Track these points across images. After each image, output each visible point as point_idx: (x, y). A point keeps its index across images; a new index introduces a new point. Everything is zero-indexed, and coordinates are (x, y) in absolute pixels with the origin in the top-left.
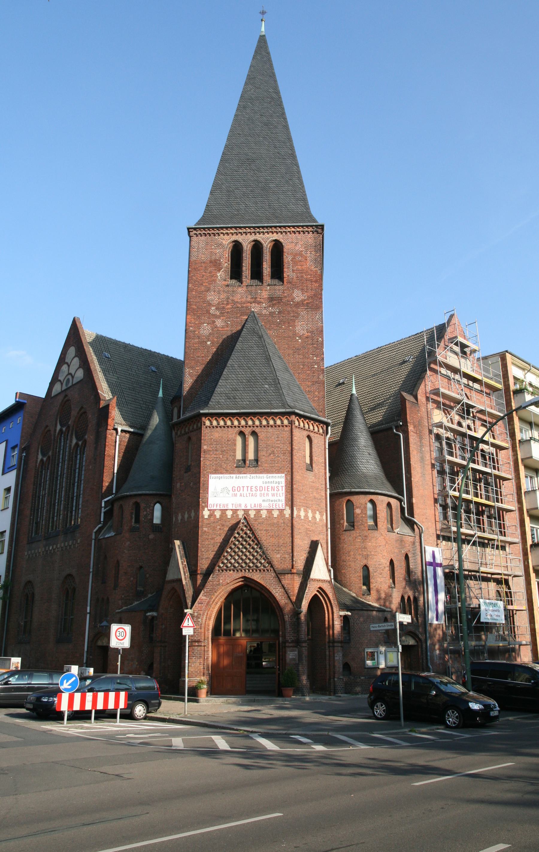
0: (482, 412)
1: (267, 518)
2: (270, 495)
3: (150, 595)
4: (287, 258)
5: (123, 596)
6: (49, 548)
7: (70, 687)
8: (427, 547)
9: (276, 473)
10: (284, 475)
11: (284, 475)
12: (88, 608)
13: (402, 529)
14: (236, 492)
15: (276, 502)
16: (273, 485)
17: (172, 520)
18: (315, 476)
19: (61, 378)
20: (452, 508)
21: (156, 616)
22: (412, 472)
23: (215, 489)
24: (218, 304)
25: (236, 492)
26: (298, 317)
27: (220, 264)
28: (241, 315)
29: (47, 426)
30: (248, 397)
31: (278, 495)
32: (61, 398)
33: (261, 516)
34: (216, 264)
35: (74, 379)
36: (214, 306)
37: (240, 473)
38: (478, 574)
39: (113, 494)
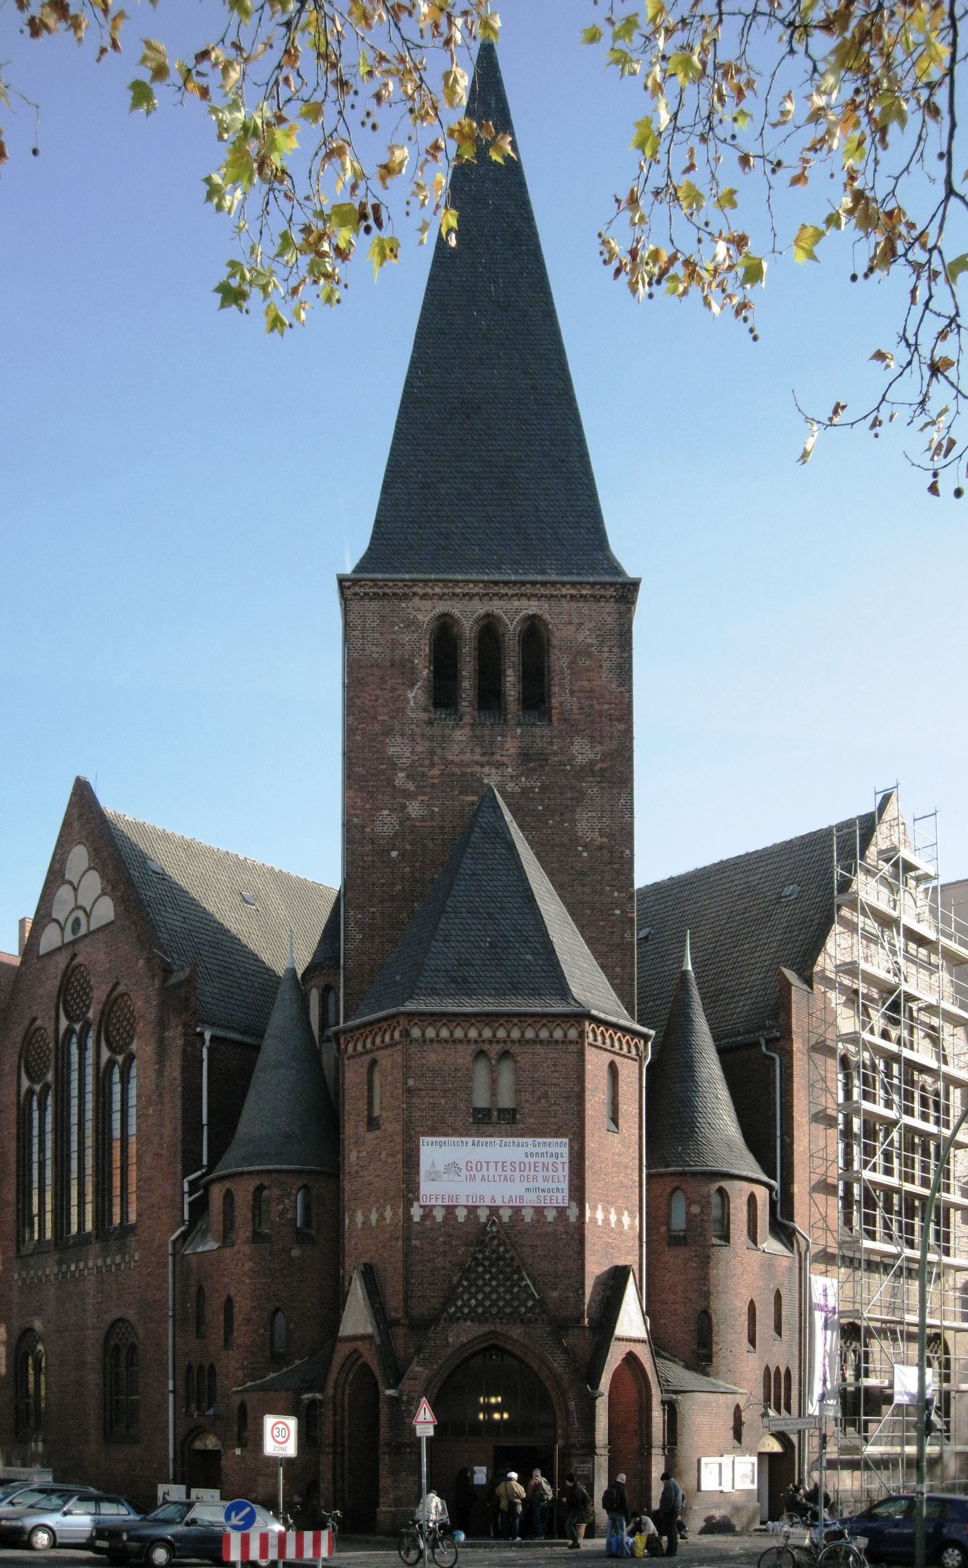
0: (931, 1009)
1: (532, 1225)
2: (540, 1179)
3: (297, 1362)
4: (559, 661)
5: (245, 1363)
6: (69, 1267)
7: (242, 1523)
8: (812, 1276)
9: (552, 1137)
10: (566, 1140)
11: (566, 1140)
12: (171, 1383)
13: (771, 1245)
14: (474, 1172)
15: (551, 1194)
16: (545, 1160)
17: (344, 1223)
18: (622, 1141)
19: (59, 912)
20: (864, 1204)
21: (320, 1401)
22: (795, 1133)
23: (433, 1165)
24: (412, 765)
25: (474, 1172)
26: (582, 801)
27: (413, 669)
28: (461, 793)
29: (34, 1019)
30: (492, 980)
31: (556, 1180)
32: (62, 960)
33: (523, 1220)
34: (404, 668)
35: (92, 920)
36: (402, 770)
37: (482, 1135)
38: (898, 1328)
39: (202, 1167)
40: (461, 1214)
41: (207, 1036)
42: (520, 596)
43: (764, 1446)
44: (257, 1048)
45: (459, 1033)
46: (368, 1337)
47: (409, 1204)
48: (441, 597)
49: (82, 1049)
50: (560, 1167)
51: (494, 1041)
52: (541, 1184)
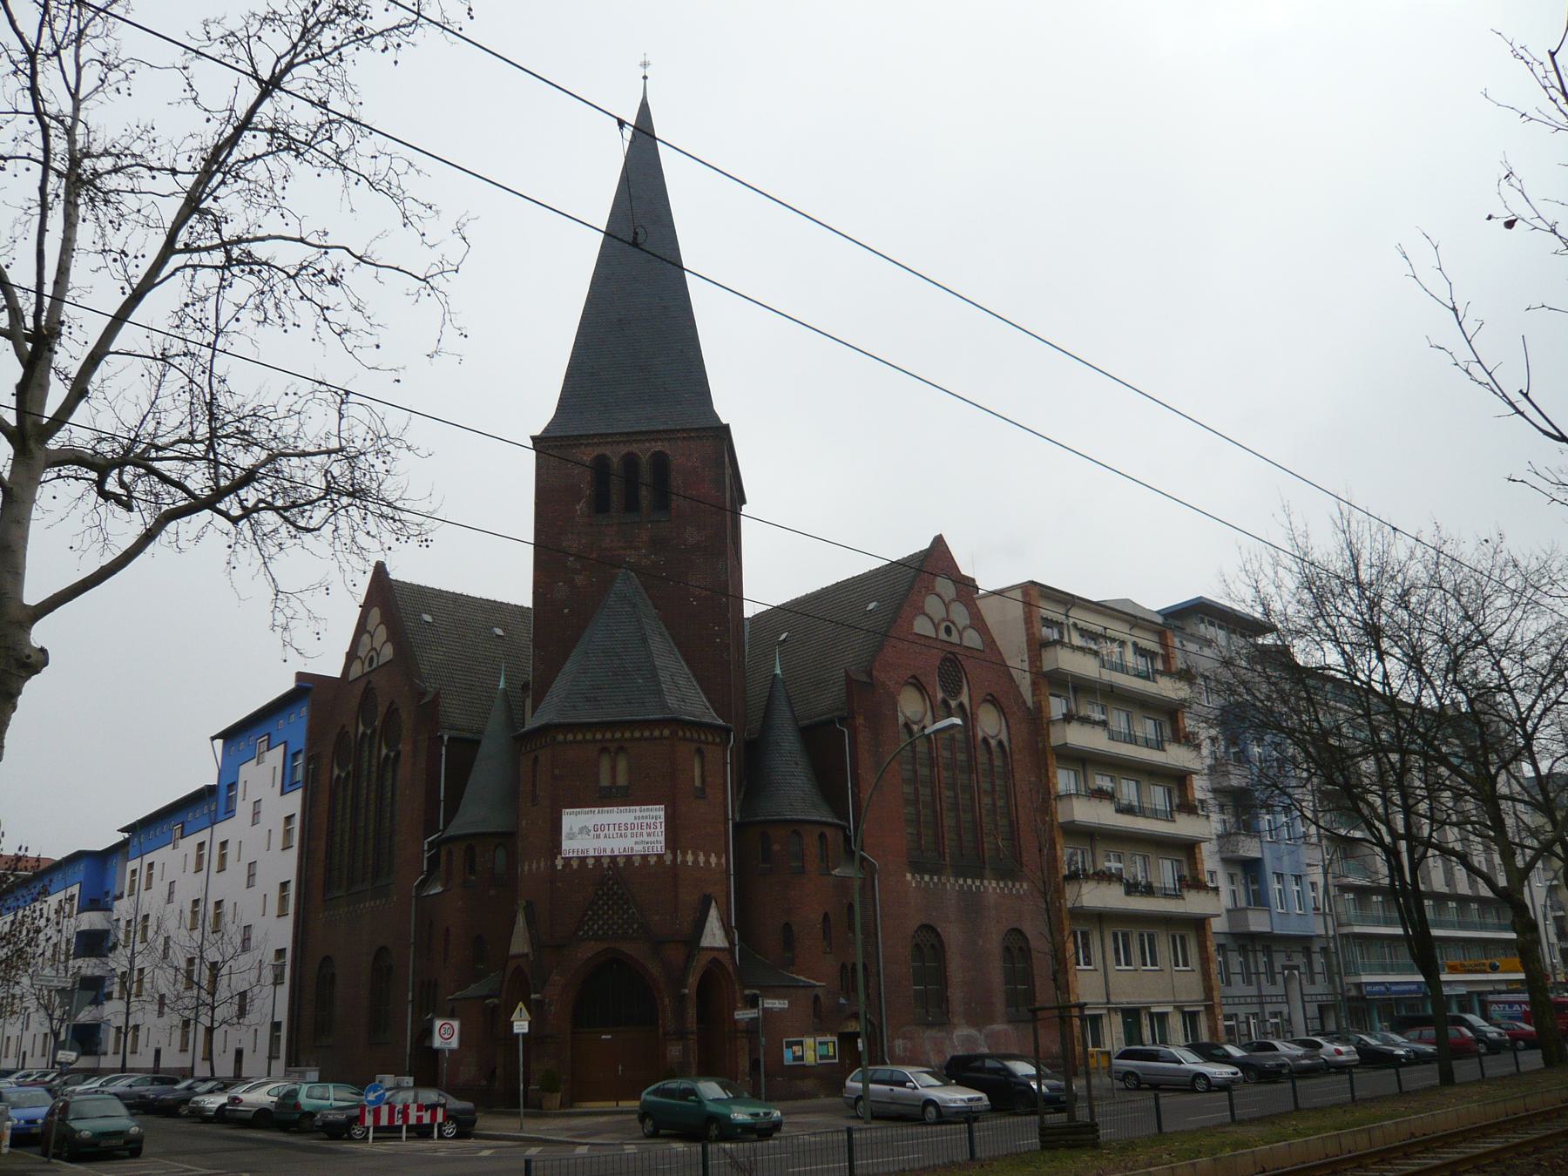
19: (362, 653)
40: (591, 862)
44: (479, 742)
45: (589, 736)
46: (526, 955)
48: (598, 445)
49: (371, 746)
51: (612, 740)
52: (646, 838)
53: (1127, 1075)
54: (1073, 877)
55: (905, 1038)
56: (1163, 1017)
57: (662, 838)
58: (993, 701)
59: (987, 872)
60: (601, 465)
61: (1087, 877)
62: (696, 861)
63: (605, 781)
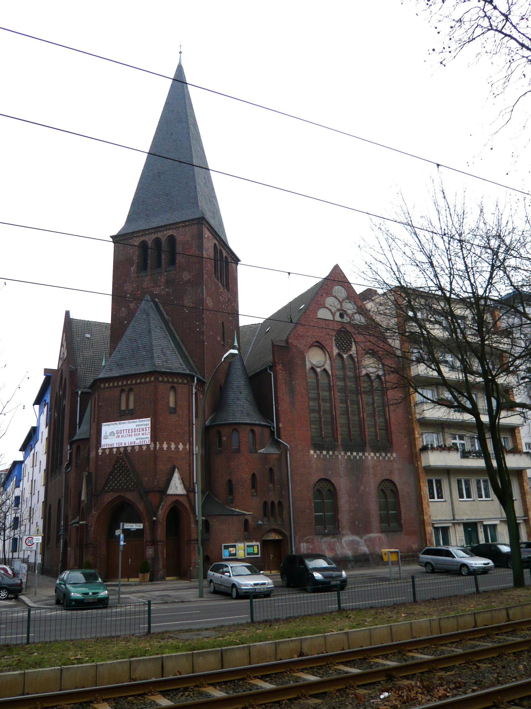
2: (141, 434)
4: (179, 248)
11: (150, 419)
12: (62, 522)
16: (143, 427)
23: (106, 433)
36: (129, 294)
40: (115, 450)
41: (80, 392)
42: (166, 230)
43: (269, 537)
47: (97, 449)
48: (142, 236)
50: (147, 429)
51: (127, 385)
52: (141, 436)
53: (427, 564)
54: (425, 449)
55: (307, 542)
56: (495, 526)
57: (149, 436)
58: (373, 353)
59: (368, 447)
60: (144, 246)
61: (433, 449)
62: (169, 448)
63: (123, 407)
